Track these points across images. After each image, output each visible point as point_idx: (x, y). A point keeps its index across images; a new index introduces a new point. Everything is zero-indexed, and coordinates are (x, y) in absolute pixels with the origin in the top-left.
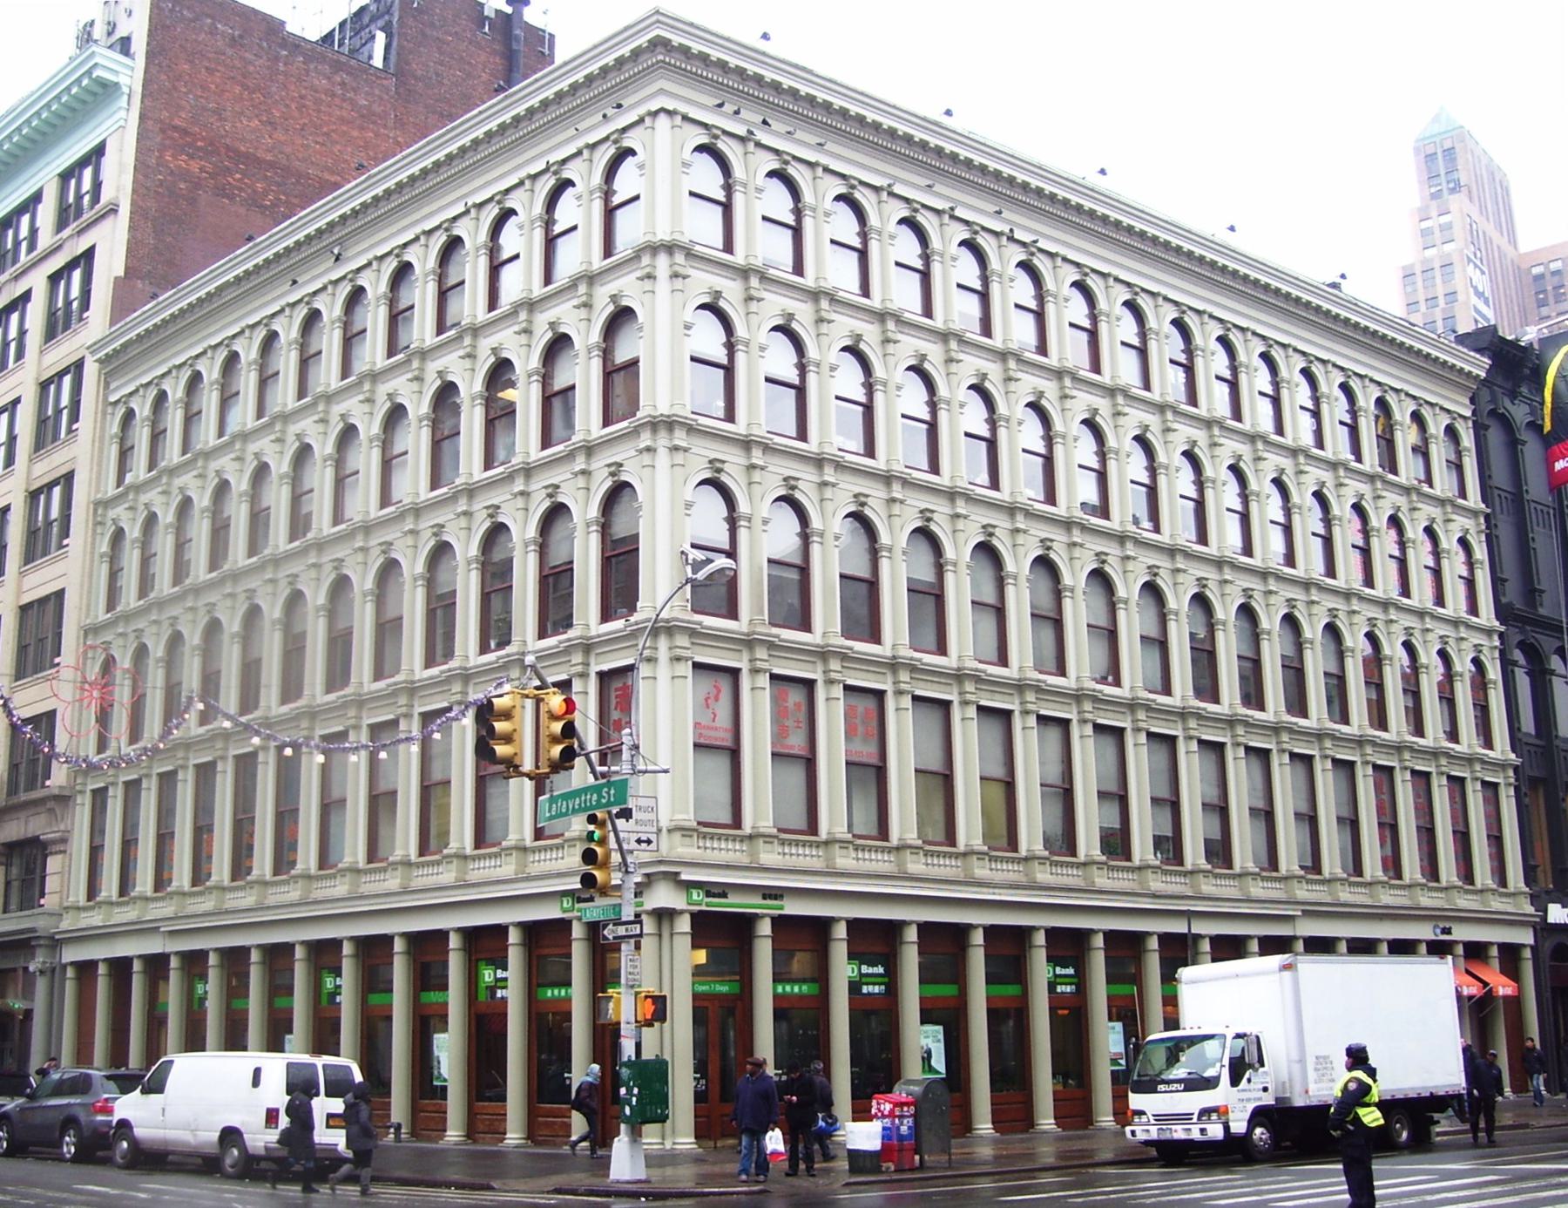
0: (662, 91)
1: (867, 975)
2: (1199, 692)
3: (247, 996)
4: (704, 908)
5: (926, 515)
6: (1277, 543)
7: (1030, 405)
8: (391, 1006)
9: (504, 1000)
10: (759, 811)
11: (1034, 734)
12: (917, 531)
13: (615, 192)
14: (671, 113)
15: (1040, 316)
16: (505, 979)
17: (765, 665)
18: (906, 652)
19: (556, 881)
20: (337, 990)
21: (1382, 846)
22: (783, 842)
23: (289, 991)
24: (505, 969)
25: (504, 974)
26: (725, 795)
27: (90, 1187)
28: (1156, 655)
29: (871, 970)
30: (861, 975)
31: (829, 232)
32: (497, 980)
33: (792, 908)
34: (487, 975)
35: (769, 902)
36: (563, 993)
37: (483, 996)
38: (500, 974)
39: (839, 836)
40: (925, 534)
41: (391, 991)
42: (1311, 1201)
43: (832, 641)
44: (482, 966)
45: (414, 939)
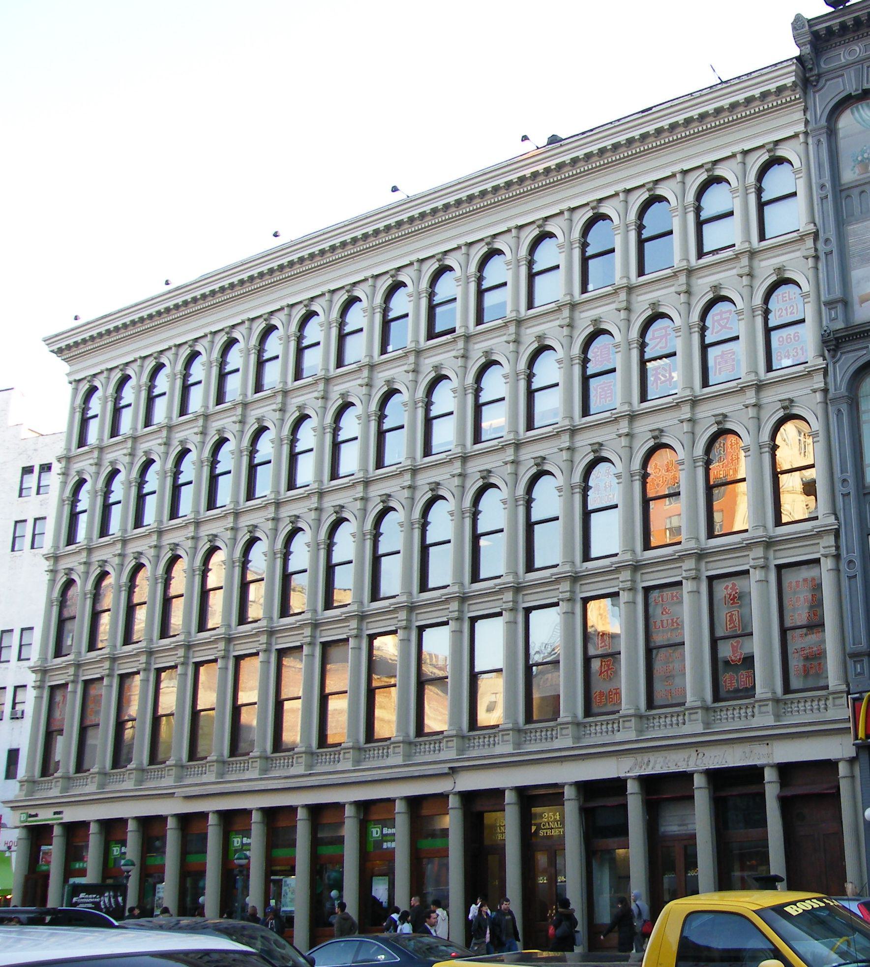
0: (826, 81)
1: (387, 835)
3: (205, 852)
8: (205, 864)
9: (392, 852)
13: (190, 375)
16: (249, 844)
20: (245, 847)
21: (502, 961)
23: (162, 851)
24: (249, 837)
25: (249, 841)
27: (488, 931)
30: (383, 835)
32: (243, 844)
34: (116, 850)
36: (81, 865)
37: (111, 864)
38: (245, 840)
41: (294, 845)
42: (486, 599)
44: (232, 835)
45: (315, 810)
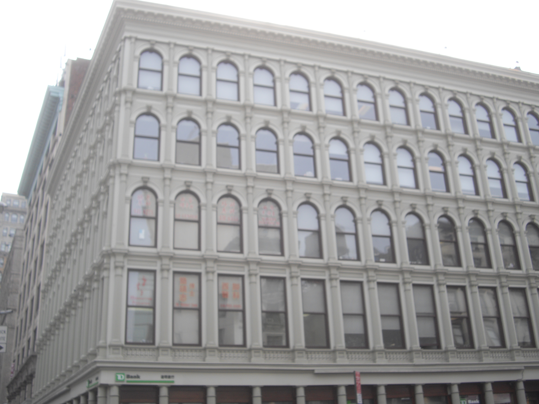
2: (413, 258)
4: (125, 383)
5: (413, 206)
6: (522, 190)
7: (516, 163)
10: (512, 341)
11: (446, 294)
12: (529, 224)
14: (130, 38)
15: (517, 128)
17: (535, 285)
18: (503, 270)
19: (379, 371)
22: (492, 352)
26: (527, 334)
28: (316, 237)
29: (473, 402)
31: (388, 103)
33: (180, 380)
35: (165, 379)
39: (514, 348)
40: (505, 223)
43: (405, 265)
